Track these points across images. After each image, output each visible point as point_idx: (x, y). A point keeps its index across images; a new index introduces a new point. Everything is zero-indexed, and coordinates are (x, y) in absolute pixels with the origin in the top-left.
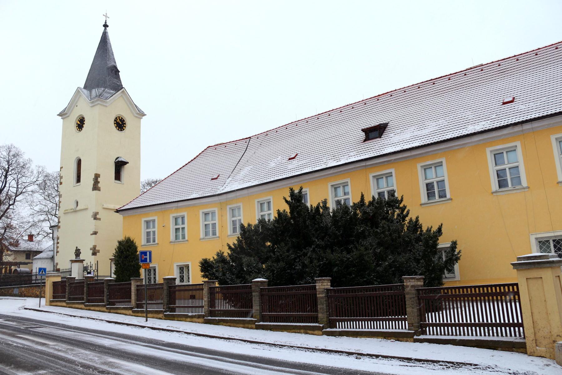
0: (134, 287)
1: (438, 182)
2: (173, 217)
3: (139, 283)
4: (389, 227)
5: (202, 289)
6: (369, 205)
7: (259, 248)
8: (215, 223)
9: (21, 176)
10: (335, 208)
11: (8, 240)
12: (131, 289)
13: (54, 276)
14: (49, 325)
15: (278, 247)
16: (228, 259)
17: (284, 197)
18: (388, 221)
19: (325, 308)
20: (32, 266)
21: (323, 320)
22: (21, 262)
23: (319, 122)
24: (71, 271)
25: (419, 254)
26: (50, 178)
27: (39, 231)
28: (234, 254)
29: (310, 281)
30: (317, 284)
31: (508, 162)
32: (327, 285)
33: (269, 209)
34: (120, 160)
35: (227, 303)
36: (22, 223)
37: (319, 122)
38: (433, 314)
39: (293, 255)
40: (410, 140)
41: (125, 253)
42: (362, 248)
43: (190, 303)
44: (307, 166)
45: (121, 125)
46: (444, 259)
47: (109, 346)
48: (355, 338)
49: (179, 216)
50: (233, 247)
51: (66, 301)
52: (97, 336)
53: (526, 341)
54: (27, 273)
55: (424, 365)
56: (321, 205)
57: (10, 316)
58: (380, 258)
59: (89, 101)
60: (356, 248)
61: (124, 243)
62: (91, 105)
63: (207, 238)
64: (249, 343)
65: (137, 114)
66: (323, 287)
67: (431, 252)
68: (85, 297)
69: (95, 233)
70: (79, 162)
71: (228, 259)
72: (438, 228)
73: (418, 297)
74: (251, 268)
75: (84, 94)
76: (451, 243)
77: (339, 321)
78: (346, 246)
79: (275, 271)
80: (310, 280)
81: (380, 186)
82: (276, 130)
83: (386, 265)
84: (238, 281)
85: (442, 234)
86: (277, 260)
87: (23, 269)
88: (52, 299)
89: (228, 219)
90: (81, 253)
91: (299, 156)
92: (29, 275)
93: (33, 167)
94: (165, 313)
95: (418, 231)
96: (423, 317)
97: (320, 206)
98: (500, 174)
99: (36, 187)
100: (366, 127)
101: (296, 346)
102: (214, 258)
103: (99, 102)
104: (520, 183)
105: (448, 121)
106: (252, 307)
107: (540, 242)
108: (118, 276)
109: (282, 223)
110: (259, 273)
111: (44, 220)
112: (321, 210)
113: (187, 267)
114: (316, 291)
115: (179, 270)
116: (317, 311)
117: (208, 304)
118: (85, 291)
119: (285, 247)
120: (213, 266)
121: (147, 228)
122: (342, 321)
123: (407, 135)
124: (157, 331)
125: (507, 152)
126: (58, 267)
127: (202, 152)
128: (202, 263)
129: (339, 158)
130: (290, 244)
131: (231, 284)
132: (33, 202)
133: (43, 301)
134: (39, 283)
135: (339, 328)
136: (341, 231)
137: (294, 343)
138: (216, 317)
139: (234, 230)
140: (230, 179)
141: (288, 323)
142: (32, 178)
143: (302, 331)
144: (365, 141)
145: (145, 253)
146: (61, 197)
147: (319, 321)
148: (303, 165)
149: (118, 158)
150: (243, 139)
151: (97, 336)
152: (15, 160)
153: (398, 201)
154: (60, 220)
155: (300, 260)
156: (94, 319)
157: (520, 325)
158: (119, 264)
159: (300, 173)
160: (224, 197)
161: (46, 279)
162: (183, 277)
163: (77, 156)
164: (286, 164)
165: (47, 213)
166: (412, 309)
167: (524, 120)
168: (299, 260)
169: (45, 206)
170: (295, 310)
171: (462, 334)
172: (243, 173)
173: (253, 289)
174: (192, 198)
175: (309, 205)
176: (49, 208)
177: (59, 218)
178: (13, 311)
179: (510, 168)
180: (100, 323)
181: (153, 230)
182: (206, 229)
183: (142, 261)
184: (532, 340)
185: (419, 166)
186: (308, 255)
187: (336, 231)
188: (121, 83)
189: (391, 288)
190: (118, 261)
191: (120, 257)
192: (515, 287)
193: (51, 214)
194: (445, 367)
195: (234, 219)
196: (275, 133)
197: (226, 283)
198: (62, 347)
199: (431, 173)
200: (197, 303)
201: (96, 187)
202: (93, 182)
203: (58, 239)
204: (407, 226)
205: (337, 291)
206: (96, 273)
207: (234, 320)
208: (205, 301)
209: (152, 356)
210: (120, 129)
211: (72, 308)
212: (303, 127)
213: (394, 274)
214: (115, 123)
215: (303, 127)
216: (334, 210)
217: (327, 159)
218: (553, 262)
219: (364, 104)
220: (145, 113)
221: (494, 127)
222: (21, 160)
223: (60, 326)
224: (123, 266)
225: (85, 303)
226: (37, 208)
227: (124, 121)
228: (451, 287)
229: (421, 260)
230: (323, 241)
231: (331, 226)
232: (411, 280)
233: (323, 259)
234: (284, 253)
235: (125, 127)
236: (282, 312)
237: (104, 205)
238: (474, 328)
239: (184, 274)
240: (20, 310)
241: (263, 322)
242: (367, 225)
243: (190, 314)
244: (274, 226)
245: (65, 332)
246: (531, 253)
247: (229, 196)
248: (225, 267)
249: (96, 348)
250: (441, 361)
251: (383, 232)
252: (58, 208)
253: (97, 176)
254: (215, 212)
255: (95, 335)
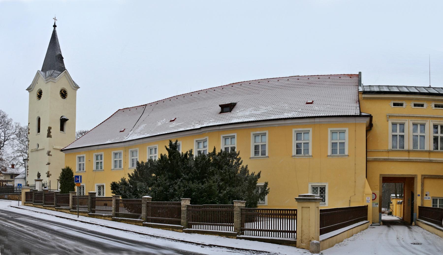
0: (71, 197)
1: (262, 145)
2: (95, 155)
3: (74, 195)
4: (229, 169)
5: (112, 200)
6: (218, 155)
7: (148, 177)
8: (121, 160)
9: (7, 129)
10: (197, 156)
11: (1, 167)
12: (69, 198)
13: (26, 189)
14: (24, 216)
15: (159, 177)
16: (128, 183)
17: (165, 146)
18: (229, 166)
19: (186, 216)
20: (14, 183)
21: (184, 223)
22: (8, 180)
23: (192, 97)
24: (35, 186)
25: (245, 188)
26: (23, 130)
27: (17, 162)
28: (132, 180)
29: (178, 199)
30: (182, 202)
31: (304, 139)
32: (188, 203)
33: (155, 153)
34: (63, 118)
35: (126, 209)
36: (8, 157)
37: (192, 97)
38: (249, 223)
39: (168, 183)
40: (249, 116)
41: (66, 176)
42: (211, 182)
43: (104, 208)
44: (182, 127)
45: (64, 95)
46: (260, 193)
47: (57, 230)
48: (203, 235)
49: (99, 154)
50: (131, 175)
51: (33, 203)
52: (50, 224)
53: (297, 240)
54: (11, 186)
55: (240, 252)
56: (189, 153)
57: (4, 210)
58: (220, 188)
59: (45, 80)
60: (208, 181)
61: (66, 170)
62: (46, 82)
63: (115, 169)
64: (138, 234)
65: (74, 87)
66: (185, 204)
67: (252, 187)
68: (43, 202)
69: (49, 164)
70: (39, 120)
71: (128, 183)
72: (258, 174)
73: (241, 213)
74: (142, 189)
75: (42, 74)
76: (264, 183)
77: (194, 224)
78: (201, 180)
79: (156, 192)
80: (178, 199)
81: (200, 147)
82: (163, 101)
83: (225, 193)
84: (134, 197)
85: (260, 177)
86: (159, 186)
87: (9, 184)
88: (25, 202)
89: (130, 158)
90: (40, 176)
91: (177, 120)
92: (13, 187)
93: (13, 123)
94: (89, 213)
95: (246, 174)
96: (243, 225)
97: (188, 154)
98: (298, 146)
99: (15, 136)
100: (222, 104)
101: (166, 237)
102: (119, 182)
103: (51, 80)
104: (308, 153)
105: (273, 108)
106: (141, 213)
107: (313, 188)
108: (62, 190)
109: (163, 163)
110: (147, 193)
111: (20, 156)
112: (188, 156)
113: (103, 186)
114: (181, 206)
115: (98, 188)
116: (180, 218)
117: (115, 210)
118: (43, 198)
119: (164, 178)
120: (119, 187)
121: (79, 161)
122: (197, 224)
123: (247, 113)
124: (84, 223)
125: (304, 133)
126: (28, 184)
127: (115, 113)
128: (112, 185)
129: (203, 122)
130: (167, 176)
131: (129, 198)
132: (13, 145)
133: (20, 202)
134: (18, 192)
135: (194, 228)
136: (200, 170)
137: (165, 236)
138: (119, 217)
139: (133, 165)
140: (132, 132)
141: (163, 224)
142: (13, 130)
143: (171, 229)
144: (221, 113)
145: (77, 177)
146: (29, 142)
147: (181, 224)
148: (179, 126)
149: (62, 117)
150: (141, 106)
151: (50, 224)
152: (3, 119)
153: (236, 154)
154: (29, 156)
155: (173, 186)
156: (48, 214)
157: (295, 232)
158: (63, 182)
159: (176, 131)
160: (128, 143)
161: (22, 190)
162: (100, 192)
163: (38, 116)
164: (168, 124)
165: (22, 151)
166: (237, 219)
167: (316, 116)
168: (172, 187)
169: (20, 147)
170: (167, 216)
171: (264, 235)
172: (140, 128)
173: (142, 202)
174: (107, 143)
175: (181, 152)
176: (23, 148)
177: (28, 154)
178: (5, 208)
179: (304, 143)
180: (52, 216)
181: (83, 163)
182: (115, 163)
183: (76, 182)
184: (300, 240)
185: (252, 133)
186: (178, 184)
187: (196, 170)
188: (64, 66)
189: (226, 207)
190: (62, 181)
191: (63, 179)
192: (295, 211)
193: (24, 152)
194: (252, 253)
195: (133, 158)
196: (163, 103)
197: (126, 197)
198: (31, 229)
199: (259, 139)
200: (108, 208)
201: (49, 136)
202: (47, 132)
203: (28, 167)
204: (240, 170)
205: (194, 207)
206: (49, 188)
207: (130, 220)
208: (113, 208)
209: (81, 237)
210: (63, 98)
211: (36, 207)
212: (181, 100)
213: (229, 198)
214: (60, 94)
215: (181, 100)
216: (196, 157)
217: (194, 123)
218: (316, 199)
219: (222, 89)
220: (79, 87)
221: (299, 117)
222: (6, 120)
223: (29, 217)
224: (65, 184)
225: (43, 205)
226: (16, 149)
227: (66, 92)
228: (260, 209)
229: (246, 191)
230: (188, 176)
231: (194, 167)
232: (238, 203)
233: (187, 186)
234: (163, 181)
235: (67, 96)
236: (160, 217)
237: (54, 146)
238: (270, 232)
239: (101, 191)
240: (8, 207)
241: (147, 222)
242: (216, 168)
243: (104, 215)
244: (158, 164)
245: (32, 221)
246: (308, 193)
247: (131, 143)
248: (126, 188)
249: (50, 231)
250: (250, 250)
251: (225, 173)
252: (27, 148)
253: (50, 128)
254: (121, 153)
255: (49, 224)
